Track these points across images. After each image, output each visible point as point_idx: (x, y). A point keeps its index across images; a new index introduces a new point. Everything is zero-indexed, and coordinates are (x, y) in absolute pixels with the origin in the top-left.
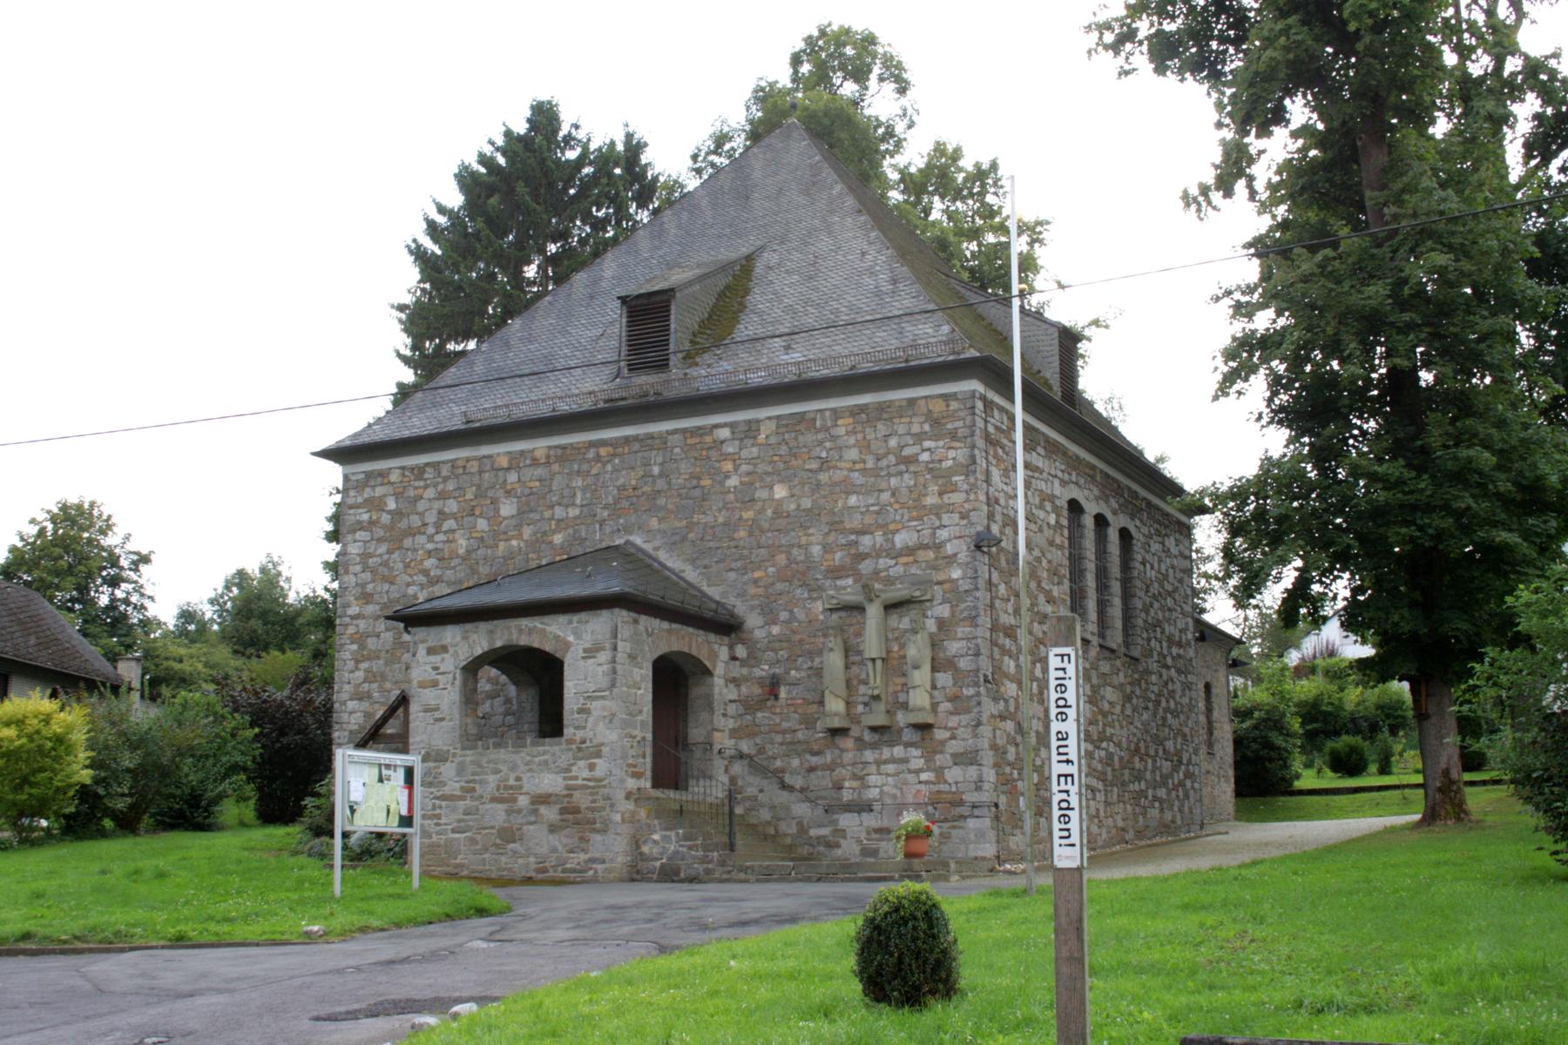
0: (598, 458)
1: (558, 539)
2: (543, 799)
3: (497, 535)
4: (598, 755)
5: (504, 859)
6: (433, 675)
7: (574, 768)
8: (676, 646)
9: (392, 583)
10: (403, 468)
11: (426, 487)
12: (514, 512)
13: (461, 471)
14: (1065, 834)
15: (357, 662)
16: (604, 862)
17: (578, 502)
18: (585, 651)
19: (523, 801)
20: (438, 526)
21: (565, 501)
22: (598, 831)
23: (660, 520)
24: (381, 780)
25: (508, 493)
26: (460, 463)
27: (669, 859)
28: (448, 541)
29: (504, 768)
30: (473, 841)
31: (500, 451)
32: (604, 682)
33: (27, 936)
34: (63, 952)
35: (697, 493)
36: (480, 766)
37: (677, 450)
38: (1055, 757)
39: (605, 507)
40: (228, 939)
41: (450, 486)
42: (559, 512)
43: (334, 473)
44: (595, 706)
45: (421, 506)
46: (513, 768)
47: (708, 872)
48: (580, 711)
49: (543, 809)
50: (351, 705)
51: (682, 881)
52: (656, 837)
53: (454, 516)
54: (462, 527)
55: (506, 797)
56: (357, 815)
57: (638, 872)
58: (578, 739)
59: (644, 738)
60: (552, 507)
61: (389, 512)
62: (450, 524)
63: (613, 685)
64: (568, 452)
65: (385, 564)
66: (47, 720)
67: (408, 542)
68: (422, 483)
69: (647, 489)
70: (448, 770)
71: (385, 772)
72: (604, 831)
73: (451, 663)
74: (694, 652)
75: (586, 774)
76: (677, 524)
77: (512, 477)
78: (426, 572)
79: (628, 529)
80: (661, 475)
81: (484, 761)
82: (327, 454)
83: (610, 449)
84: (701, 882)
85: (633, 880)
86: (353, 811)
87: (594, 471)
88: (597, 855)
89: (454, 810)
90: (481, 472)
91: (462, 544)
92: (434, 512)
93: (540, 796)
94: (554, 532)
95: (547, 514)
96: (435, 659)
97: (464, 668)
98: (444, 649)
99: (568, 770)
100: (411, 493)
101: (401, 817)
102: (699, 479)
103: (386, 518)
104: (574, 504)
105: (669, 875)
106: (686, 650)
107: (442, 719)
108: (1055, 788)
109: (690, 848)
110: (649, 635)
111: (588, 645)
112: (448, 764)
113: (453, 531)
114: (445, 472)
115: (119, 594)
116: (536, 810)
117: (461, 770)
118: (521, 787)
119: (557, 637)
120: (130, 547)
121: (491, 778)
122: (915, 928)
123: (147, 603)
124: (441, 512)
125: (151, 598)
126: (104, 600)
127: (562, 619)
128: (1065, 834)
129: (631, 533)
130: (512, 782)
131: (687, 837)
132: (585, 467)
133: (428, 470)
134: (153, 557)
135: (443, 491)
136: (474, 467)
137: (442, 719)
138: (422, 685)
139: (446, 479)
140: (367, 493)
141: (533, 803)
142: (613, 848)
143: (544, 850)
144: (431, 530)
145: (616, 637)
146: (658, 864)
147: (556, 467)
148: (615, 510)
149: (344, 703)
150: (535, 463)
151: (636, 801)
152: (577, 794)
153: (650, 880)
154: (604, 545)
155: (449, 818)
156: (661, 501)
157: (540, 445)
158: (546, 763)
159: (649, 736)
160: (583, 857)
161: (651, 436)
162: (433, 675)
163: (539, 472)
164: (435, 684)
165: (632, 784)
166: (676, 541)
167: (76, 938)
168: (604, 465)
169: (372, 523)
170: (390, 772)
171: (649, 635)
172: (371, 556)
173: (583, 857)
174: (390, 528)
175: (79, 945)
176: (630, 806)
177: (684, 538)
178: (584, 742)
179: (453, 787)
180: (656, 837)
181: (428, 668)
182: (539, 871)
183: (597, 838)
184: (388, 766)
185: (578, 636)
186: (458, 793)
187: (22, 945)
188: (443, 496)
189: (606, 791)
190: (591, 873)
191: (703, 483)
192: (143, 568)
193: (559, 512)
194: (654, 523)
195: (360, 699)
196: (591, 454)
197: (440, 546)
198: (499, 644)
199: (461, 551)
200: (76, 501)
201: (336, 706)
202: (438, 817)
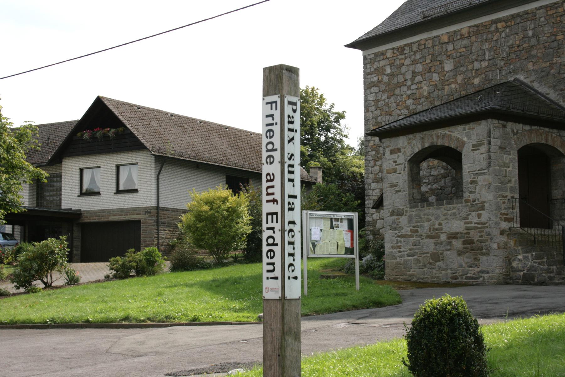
0: (497, 29)
1: (476, 81)
2: (453, 236)
3: (444, 82)
4: (483, 208)
5: (434, 271)
6: (394, 166)
7: (470, 217)
8: (535, 140)
9: (391, 115)
10: (393, 49)
11: (405, 58)
12: (452, 68)
13: (423, 47)
14: (271, 267)
15: (375, 161)
16: (488, 273)
17: (487, 58)
18: (474, 146)
19: (443, 237)
20: (412, 80)
21: (480, 58)
22: (484, 254)
23: (534, 64)
24: (332, 227)
25: (449, 57)
26: (423, 42)
27: (528, 270)
28: (418, 88)
29: (432, 218)
30: (418, 261)
31: (443, 32)
32: (484, 164)
33: (127, 318)
34: (141, 327)
35: (555, 44)
36: (420, 217)
37: (542, 19)
38: (265, 198)
39: (503, 59)
40: (218, 320)
41: (418, 56)
42: (477, 65)
43: (358, 54)
44: (480, 179)
45: (403, 70)
46: (437, 218)
47: (551, 278)
48: (472, 182)
49: (454, 242)
50: (373, 185)
51: (536, 284)
52: (520, 257)
53: (420, 74)
54: (425, 79)
55: (434, 235)
56: (317, 249)
57: (511, 278)
58: (471, 199)
59: (513, 197)
60: (472, 63)
61: (387, 75)
62: (418, 78)
63: (489, 166)
64: (480, 28)
65: (386, 105)
66: (225, 200)
67: (397, 91)
68: (403, 56)
69: (525, 45)
70: (403, 220)
71: (334, 223)
72: (487, 254)
73: (402, 158)
74: (550, 143)
75: (476, 220)
76: (544, 65)
77: (450, 47)
78: (407, 108)
79: (515, 72)
80: (533, 36)
81: (422, 213)
82: (353, 45)
83: (504, 24)
84: (546, 285)
85: (507, 283)
86: (314, 245)
87: (495, 38)
88: (484, 268)
89: (408, 243)
90: (433, 46)
91: (425, 89)
92: (410, 72)
93: (452, 234)
94: (474, 77)
95: (470, 67)
96: (394, 156)
97: (409, 161)
98: (399, 150)
99: (466, 218)
100: (398, 62)
101: (346, 248)
102: (556, 35)
103: (386, 79)
104: (484, 60)
105: (528, 280)
106: (543, 142)
107: (399, 191)
108: (265, 226)
109: (540, 264)
110: (514, 134)
111: (475, 143)
112: (403, 217)
113: (420, 82)
114: (415, 49)
115: (330, 135)
116: (451, 242)
117: (410, 220)
118: (442, 229)
119: (457, 139)
120: (334, 110)
121: (426, 224)
122: (440, 331)
123: (344, 139)
124: (414, 72)
125: (346, 136)
126: (323, 139)
127: (460, 128)
128: (271, 267)
129: (517, 74)
130: (437, 226)
131: (538, 257)
132: (490, 36)
133: (406, 48)
134: (346, 114)
135: (414, 59)
136: (429, 44)
137: (399, 191)
138: (389, 172)
139: (415, 52)
140: (376, 65)
141: (448, 238)
142: (493, 264)
143: (455, 266)
144: (409, 83)
145: (490, 137)
146: (522, 273)
147: (474, 38)
148: (508, 60)
149: (370, 185)
150: (462, 37)
151: (508, 235)
152: (472, 232)
153: (518, 284)
154: (502, 82)
155: (406, 248)
156: (534, 52)
157: (464, 26)
158: (454, 214)
159: (517, 196)
160: (477, 269)
161: (527, 13)
162: (394, 166)
163: (465, 42)
164: (395, 171)
165: (505, 225)
166: (543, 76)
167: (149, 319)
168: (501, 34)
169: (379, 82)
170: (339, 223)
171: (514, 134)
172: (379, 101)
173: (477, 269)
174: (388, 84)
175: (149, 323)
176: (504, 239)
177: (548, 74)
178: (474, 201)
179: (406, 230)
180: (520, 257)
181: (391, 162)
182: (453, 278)
183: (484, 258)
184: (337, 220)
185: (469, 137)
186: (409, 233)
187: (124, 323)
188: (414, 63)
189: (488, 230)
190: (481, 279)
191: (558, 38)
192: (342, 121)
193: (477, 65)
194: (530, 66)
195: (378, 182)
196: (493, 28)
197: (414, 91)
198: (427, 145)
199: (425, 94)
200: (305, 89)
201: (366, 186)
202: (400, 247)
